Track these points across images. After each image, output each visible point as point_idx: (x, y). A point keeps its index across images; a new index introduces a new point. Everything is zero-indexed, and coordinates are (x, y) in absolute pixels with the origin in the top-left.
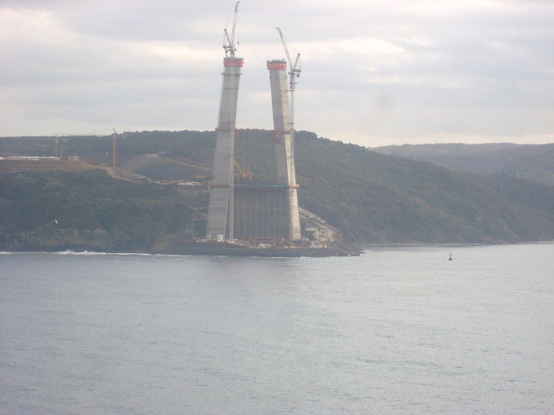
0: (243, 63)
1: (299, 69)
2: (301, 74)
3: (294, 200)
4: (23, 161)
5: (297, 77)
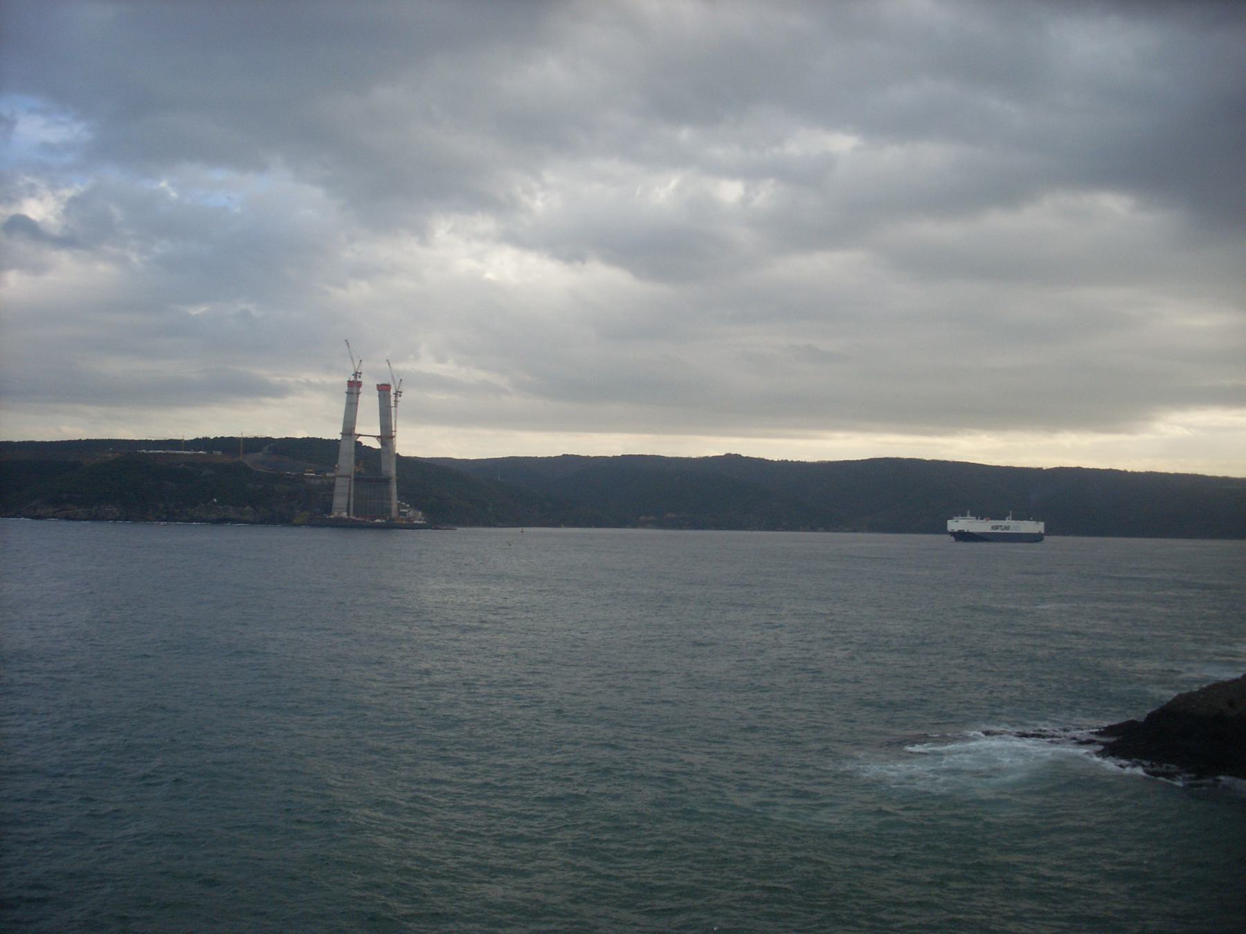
2: (402, 394)
4: (179, 454)
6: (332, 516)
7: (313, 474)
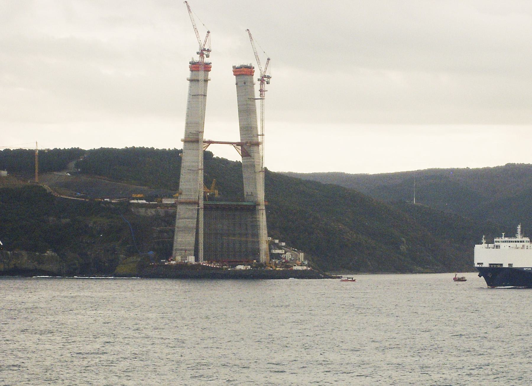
0: (211, 68)
1: (209, 48)
2: (271, 80)
3: (262, 219)
5: (267, 84)
6: (173, 262)
7: (144, 201)
